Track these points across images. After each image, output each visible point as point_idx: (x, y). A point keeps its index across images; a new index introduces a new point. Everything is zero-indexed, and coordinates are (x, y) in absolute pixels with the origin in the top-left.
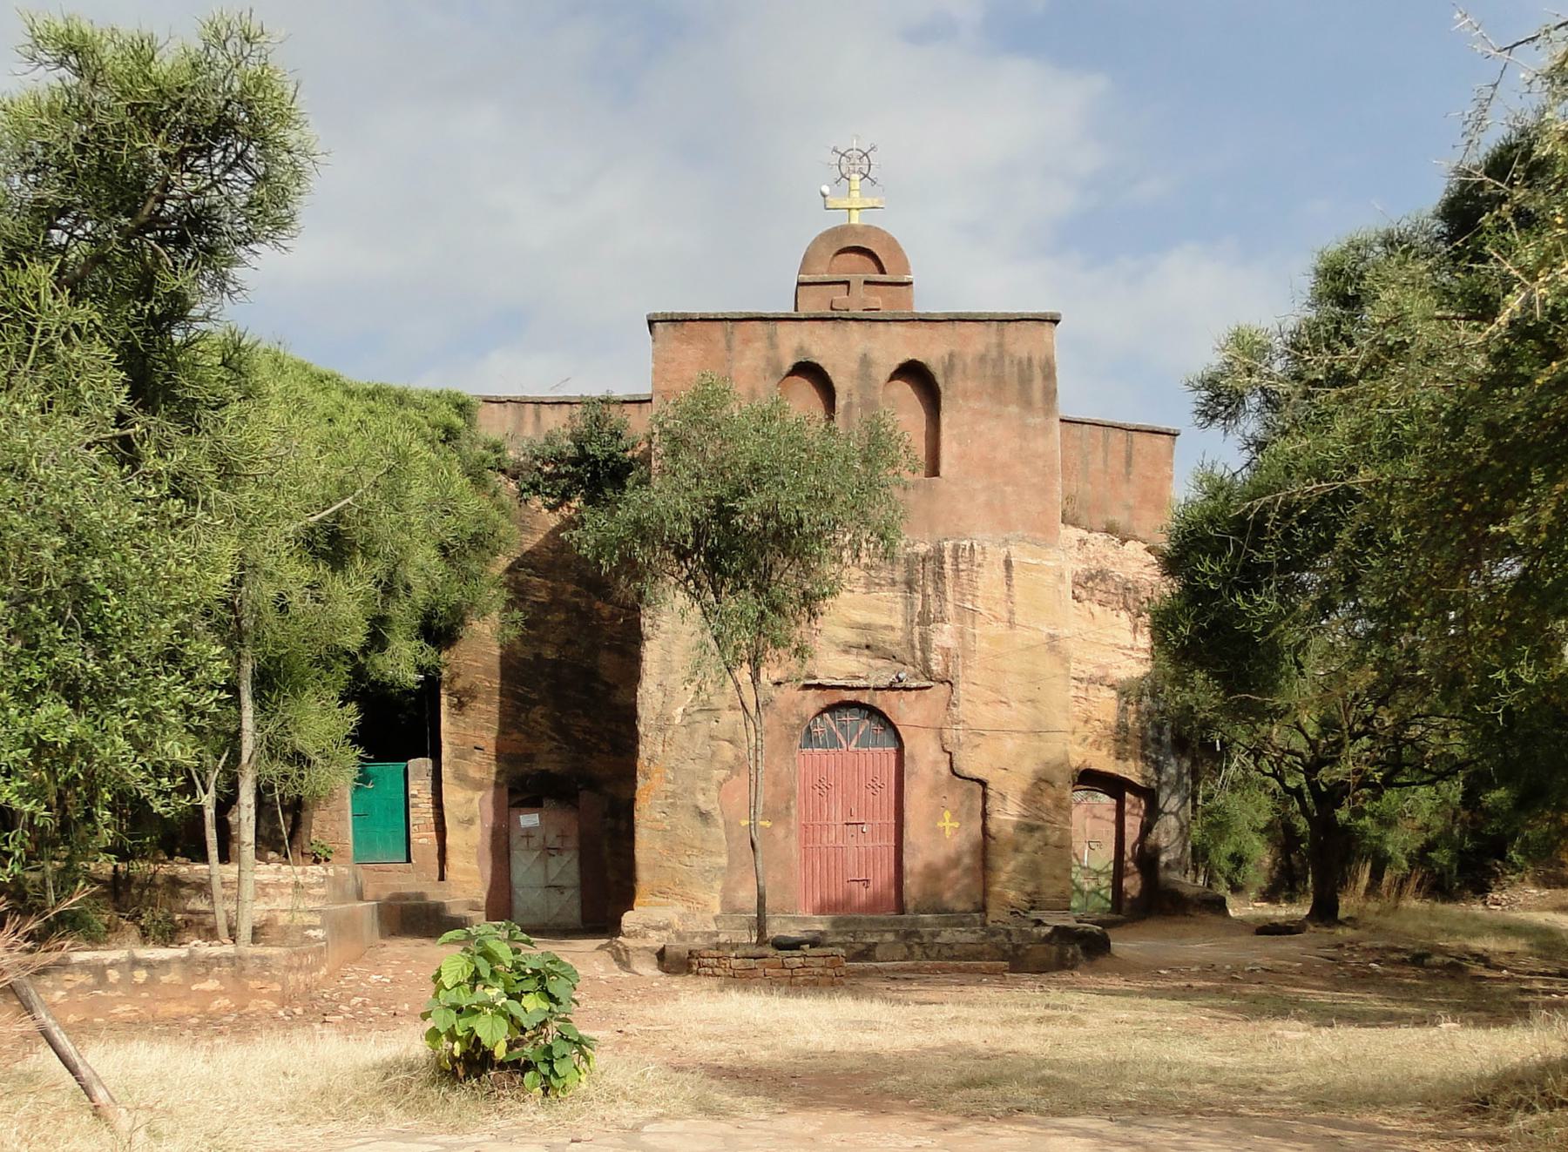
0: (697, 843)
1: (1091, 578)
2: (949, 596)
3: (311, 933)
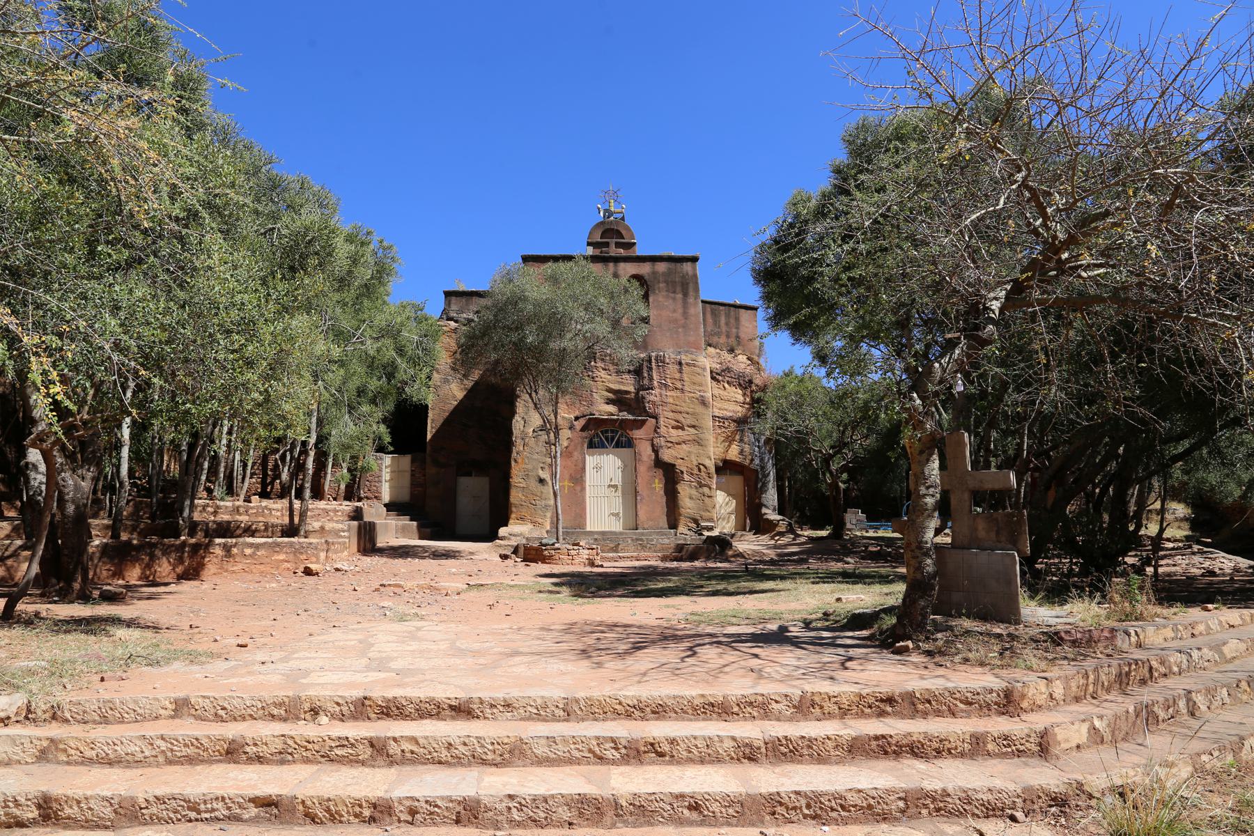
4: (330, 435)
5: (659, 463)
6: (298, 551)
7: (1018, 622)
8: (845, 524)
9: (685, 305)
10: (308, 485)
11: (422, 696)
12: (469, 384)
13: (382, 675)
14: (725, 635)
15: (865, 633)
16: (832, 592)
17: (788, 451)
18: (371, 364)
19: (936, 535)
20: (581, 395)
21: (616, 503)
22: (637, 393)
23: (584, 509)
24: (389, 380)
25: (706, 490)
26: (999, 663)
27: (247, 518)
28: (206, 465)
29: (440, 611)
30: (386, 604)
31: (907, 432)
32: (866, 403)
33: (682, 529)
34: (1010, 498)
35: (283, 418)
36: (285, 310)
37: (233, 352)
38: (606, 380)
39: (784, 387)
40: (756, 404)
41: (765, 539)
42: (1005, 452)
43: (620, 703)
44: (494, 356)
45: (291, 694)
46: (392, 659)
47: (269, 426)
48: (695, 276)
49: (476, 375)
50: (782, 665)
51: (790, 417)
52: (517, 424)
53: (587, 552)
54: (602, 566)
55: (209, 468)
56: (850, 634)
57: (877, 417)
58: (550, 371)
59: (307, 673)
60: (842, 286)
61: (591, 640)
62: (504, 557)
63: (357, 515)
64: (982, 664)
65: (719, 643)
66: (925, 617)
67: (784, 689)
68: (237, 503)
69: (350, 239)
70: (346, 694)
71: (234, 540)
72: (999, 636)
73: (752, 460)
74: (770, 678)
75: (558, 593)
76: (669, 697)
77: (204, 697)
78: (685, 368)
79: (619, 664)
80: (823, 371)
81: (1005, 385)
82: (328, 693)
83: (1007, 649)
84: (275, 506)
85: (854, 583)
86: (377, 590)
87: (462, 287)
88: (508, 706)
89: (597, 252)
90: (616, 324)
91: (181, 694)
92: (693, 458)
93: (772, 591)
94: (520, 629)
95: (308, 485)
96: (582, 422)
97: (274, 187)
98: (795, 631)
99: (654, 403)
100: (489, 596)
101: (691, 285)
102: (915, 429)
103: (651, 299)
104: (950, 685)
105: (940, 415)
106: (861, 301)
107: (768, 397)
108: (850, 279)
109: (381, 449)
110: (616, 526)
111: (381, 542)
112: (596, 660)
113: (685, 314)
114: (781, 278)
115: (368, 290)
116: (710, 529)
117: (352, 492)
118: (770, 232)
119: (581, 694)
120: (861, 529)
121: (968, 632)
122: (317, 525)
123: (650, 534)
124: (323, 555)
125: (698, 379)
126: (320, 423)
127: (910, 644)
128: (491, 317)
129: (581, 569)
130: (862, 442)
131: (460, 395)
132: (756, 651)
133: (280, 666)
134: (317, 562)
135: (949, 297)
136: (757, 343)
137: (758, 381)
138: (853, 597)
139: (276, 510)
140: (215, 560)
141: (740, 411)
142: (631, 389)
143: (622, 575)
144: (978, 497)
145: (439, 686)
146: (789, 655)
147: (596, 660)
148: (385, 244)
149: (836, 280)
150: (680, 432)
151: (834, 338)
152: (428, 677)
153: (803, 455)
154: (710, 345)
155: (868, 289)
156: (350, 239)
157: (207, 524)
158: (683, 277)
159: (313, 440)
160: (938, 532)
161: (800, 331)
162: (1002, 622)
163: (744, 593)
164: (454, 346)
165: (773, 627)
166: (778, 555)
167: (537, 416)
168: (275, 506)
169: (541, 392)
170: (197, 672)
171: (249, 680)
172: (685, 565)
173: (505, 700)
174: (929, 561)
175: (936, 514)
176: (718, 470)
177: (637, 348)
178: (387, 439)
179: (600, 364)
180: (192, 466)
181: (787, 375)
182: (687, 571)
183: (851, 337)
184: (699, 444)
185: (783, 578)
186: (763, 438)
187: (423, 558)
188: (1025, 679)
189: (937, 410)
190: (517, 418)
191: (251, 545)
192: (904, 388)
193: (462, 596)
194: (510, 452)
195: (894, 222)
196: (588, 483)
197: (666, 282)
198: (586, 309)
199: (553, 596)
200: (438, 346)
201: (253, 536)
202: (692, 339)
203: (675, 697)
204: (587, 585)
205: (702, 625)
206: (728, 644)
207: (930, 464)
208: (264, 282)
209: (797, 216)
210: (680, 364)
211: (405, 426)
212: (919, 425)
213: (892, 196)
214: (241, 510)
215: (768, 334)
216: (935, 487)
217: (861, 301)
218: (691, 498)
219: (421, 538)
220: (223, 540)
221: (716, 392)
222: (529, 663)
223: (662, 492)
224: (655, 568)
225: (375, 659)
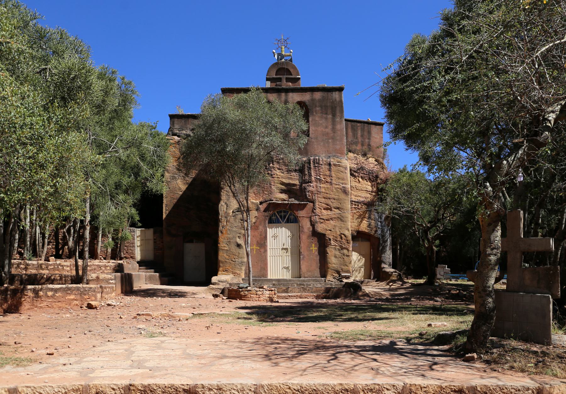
0: (237, 254)
1: (359, 169)
2: (313, 174)
3: (111, 281)
4: (99, 215)
5: (315, 233)
6: (82, 293)
7: (549, 344)
8: (436, 275)
9: (334, 123)
10: (87, 249)
11: (166, 384)
12: (189, 180)
13: (141, 371)
14: (356, 347)
15: (446, 347)
16: (426, 320)
17: (400, 225)
18: (124, 166)
19: (496, 282)
20: (264, 187)
21: (287, 260)
22: (301, 186)
23: (266, 264)
24: (136, 178)
25: (345, 251)
26: (534, 371)
27: (47, 272)
28: (17, 236)
29: (176, 330)
30: (141, 326)
31: (481, 210)
32: (454, 190)
33: (329, 277)
34: (550, 258)
35: (68, 204)
36: (62, 129)
37: (30, 158)
38: (280, 176)
39: (399, 180)
40: (380, 193)
41: (383, 285)
42: (549, 225)
43: (289, 388)
44: (206, 160)
45: (83, 383)
46: (147, 361)
47: (59, 209)
48: (341, 101)
49: (193, 174)
50: (392, 366)
51: (402, 201)
52: (222, 207)
53: (268, 292)
54: (278, 302)
55: (19, 239)
56: (436, 348)
57: (461, 199)
58: (242, 171)
59: (93, 370)
60: (443, 106)
61: (271, 349)
62: (215, 296)
63: (119, 269)
64: (523, 371)
65: (352, 351)
66: (486, 337)
67: (392, 381)
68: (40, 262)
69: (101, 76)
70: (119, 383)
71: (40, 287)
72: (535, 353)
73: (376, 231)
74: (384, 374)
75: (250, 319)
76: (320, 385)
77: (27, 387)
78: (333, 168)
79: (289, 364)
80: (426, 168)
81: (553, 176)
82: (107, 382)
83: (540, 362)
84: (65, 264)
85: (440, 314)
86: (135, 318)
87: (181, 112)
88: (220, 389)
89: (274, 85)
90: (286, 136)
91: (12, 386)
92: (337, 230)
93: (387, 318)
94: (226, 342)
95: (87, 249)
96: (265, 205)
97: (41, 37)
98: (401, 345)
99: (312, 192)
100: (206, 321)
101: (338, 109)
102: (486, 208)
103: (310, 119)
104: (500, 383)
105: (505, 199)
106: (455, 117)
107: (388, 187)
108: (449, 101)
109: (133, 225)
110: (287, 275)
111: (136, 287)
112: (274, 361)
113: (334, 129)
114: (401, 102)
115: (118, 114)
116: (348, 278)
117: (116, 254)
118: (395, 68)
119: (265, 382)
120: (446, 279)
121: (514, 349)
122: (94, 276)
123: (309, 281)
124: (99, 295)
125: (341, 175)
126: (92, 207)
127: (475, 355)
128: (203, 133)
129: (265, 304)
130: (451, 218)
131: (184, 187)
132: (375, 357)
133: (75, 366)
134: (96, 300)
135: (519, 111)
136: (382, 149)
137: (382, 176)
138: (439, 324)
139: (67, 266)
140: (28, 300)
141: (368, 197)
142: (297, 182)
143: (291, 307)
144: (528, 256)
145: (177, 377)
146: (396, 360)
147: (274, 361)
148: (126, 80)
149: (439, 101)
150: (329, 212)
151: (435, 145)
152: (169, 372)
153: (411, 228)
154: (350, 151)
155: (461, 108)
156: (101, 76)
157: (21, 276)
158: (333, 102)
159: (88, 218)
160: (497, 280)
161: (412, 140)
162: (538, 343)
163: (369, 320)
164: (178, 153)
165: (386, 342)
166: (391, 295)
167: (235, 202)
168: (65, 264)
169: (237, 185)
170: (21, 371)
171: (56, 375)
172: (331, 301)
173: (218, 386)
174: (490, 300)
175: (497, 268)
176: (354, 238)
177: (301, 154)
178: (137, 218)
179: (276, 165)
180: (8, 237)
181: (401, 172)
182: (332, 305)
183: (447, 144)
184: (342, 220)
185: (394, 310)
186: (384, 216)
187: (164, 297)
188: (552, 382)
189: (504, 195)
190: (222, 203)
191: (52, 290)
192: (481, 178)
193: (189, 321)
194: (218, 226)
195: (485, 56)
196: (268, 247)
197: (321, 106)
198: (265, 127)
199: (247, 321)
200: (167, 154)
201: (52, 283)
202: (338, 147)
203: (324, 385)
204: (267, 314)
205: (341, 340)
206: (357, 352)
207: (495, 233)
208: (45, 108)
209: (414, 55)
210: (330, 165)
211: (148, 208)
212: (489, 205)
213: (485, 36)
214: (44, 266)
215: (390, 143)
216: (498, 249)
217: (455, 117)
218: (335, 257)
219: (162, 284)
220: (33, 287)
221: (354, 184)
222: (233, 363)
223: (317, 253)
224: (312, 303)
225: (136, 361)
